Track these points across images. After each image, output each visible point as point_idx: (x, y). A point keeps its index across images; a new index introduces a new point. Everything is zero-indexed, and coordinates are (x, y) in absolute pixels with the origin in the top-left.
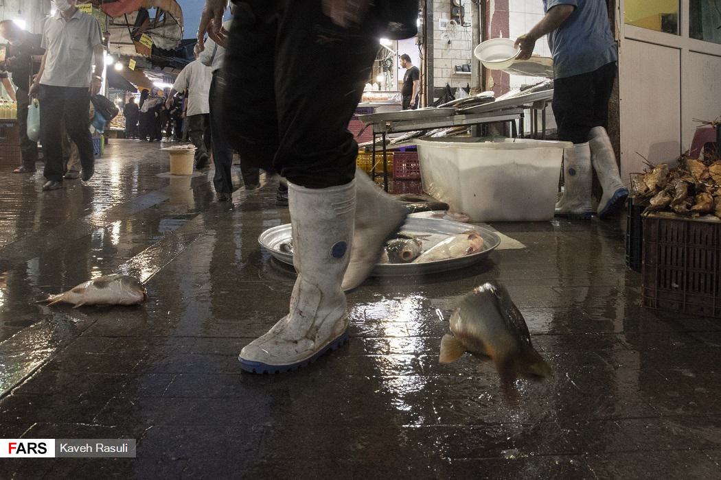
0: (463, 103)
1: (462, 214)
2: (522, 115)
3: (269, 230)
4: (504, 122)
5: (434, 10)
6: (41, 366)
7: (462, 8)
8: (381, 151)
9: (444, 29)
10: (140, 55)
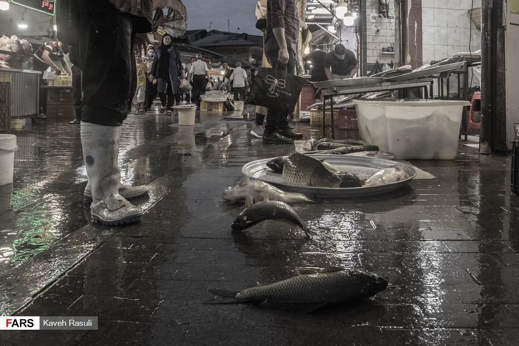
0: (389, 74)
1: (389, 153)
2: (432, 82)
3: (247, 164)
4: (419, 88)
5: (367, 7)
6: (86, 256)
7: (387, 6)
8: (329, 109)
9: (374, 21)
10: (157, 41)
